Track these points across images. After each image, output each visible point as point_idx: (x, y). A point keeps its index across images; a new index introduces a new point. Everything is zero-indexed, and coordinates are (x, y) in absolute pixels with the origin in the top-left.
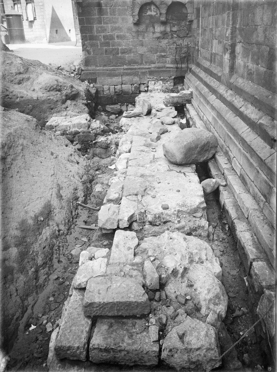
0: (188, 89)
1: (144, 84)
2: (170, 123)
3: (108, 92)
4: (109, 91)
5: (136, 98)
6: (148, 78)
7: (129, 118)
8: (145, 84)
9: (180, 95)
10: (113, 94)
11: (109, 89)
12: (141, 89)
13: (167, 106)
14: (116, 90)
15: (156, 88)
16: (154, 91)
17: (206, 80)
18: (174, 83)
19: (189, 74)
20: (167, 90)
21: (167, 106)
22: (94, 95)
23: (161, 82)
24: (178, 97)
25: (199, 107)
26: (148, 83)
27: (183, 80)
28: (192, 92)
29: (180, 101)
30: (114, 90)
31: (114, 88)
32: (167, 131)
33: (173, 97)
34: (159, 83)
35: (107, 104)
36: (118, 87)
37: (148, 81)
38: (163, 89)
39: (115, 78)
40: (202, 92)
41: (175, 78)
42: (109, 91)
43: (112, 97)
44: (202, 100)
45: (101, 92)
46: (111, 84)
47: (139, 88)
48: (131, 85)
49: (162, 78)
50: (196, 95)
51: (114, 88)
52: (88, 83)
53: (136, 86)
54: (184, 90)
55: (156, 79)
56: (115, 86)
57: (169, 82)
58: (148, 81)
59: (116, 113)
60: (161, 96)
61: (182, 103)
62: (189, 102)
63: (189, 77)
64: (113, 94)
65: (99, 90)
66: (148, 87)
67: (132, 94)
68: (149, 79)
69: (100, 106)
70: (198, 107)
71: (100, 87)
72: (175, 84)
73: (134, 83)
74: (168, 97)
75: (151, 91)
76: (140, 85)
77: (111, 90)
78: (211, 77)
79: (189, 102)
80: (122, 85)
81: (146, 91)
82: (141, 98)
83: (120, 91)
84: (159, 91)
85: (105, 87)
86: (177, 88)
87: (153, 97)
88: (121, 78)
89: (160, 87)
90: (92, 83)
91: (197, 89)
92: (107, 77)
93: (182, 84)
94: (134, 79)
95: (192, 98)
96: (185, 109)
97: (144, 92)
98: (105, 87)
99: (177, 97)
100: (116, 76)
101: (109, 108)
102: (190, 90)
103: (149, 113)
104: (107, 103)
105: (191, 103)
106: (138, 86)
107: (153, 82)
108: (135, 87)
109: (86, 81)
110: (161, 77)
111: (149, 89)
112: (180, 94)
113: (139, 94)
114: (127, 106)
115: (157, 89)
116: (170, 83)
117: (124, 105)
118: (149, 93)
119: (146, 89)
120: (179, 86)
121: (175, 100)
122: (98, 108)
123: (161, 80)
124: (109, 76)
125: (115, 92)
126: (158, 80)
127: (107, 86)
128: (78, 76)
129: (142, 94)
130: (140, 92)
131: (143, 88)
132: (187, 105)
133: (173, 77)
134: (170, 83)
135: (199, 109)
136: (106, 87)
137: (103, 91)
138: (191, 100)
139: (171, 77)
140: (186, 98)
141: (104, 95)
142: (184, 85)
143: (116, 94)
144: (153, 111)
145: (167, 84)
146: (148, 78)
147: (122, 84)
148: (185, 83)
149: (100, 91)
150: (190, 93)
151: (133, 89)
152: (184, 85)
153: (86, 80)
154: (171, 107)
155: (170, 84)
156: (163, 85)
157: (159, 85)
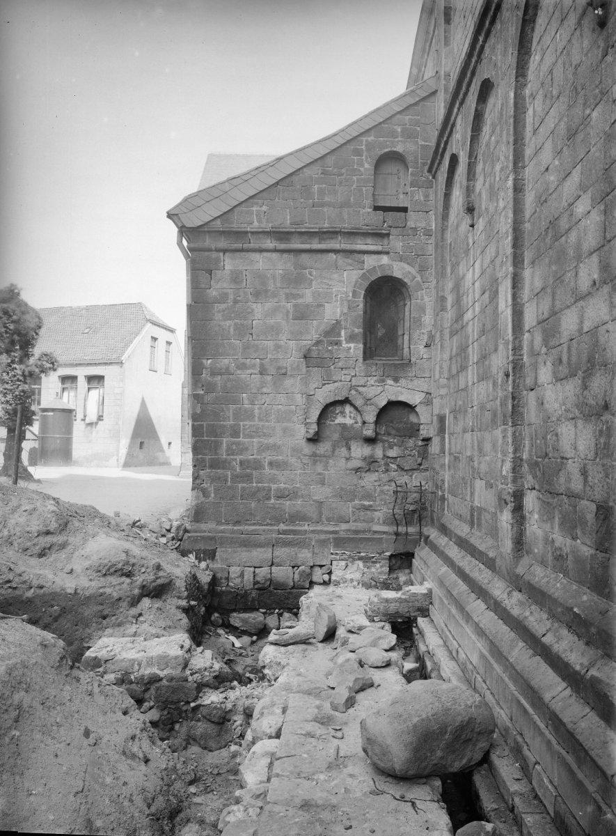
0: (421, 584)
1: (321, 566)
2: (379, 665)
3: (238, 581)
4: (240, 579)
5: (302, 598)
6: (332, 554)
7: (283, 646)
8: (324, 566)
9: (403, 597)
10: (249, 586)
11: (242, 575)
12: (315, 579)
13: (374, 621)
14: (258, 579)
15: (348, 577)
16: (344, 582)
17: (461, 564)
18: (389, 567)
19: (423, 548)
20: (373, 583)
21: (374, 621)
22: (206, 587)
23: (361, 564)
24: (400, 600)
25: (446, 626)
26: (331, 565)
27: (411, 563)
28: (430, 591)
29: (403, 609)
30: (252, 578)
31: (254, 572)
32: (372, 685)
33: (387, 601)
34: (355, 566)
35: (234, 610)
36: (263, 573)
37: (332, 561)
38: (366, 579)
39: (258, 549)
40: (454, 593)
41: (391, 556)
42: (240, 579)
43: (246, 595)
44: (454, 611)
45: (223, 581)
46: (248, 565)
47: (310, 574)
48: (293, 567)
49: (362, 554)
50: (440, 598)
51: (254, 572)
52: (196, 558)
53: (304, 571)
54: (412, 585)
55: (350, 557)
56: (255, 567)
57: (378, 565)
58: (332, 561)
59: (253, 631)
60: (360, 596)
61: (407, 615)
62: (425, 612)
63: (423, 555)
64: (249, 586)
65: (219, 575)
66: (330, 573)
67: (293, 587)
68: (332, 556)
69: (216, 615)
70: (444, 627)
71: (223, 570)
72: (391, 570)
73: (299, 564)
74: (376, 600)
75: (337, 584)
76: (312, 567)
77: (246, 577)
78: (473, 559)
79: (425, 612)
80: (273, 568)
81: (325, 583)
82: (312, 599)
83: (266, 580)
84: (355, 583)
85: (232, 569)
86: (397, 578)
87: (340, 597)
88: (270, 550)
89: (357, 576)
90: (205, 560)
91: (441, 583)
92: (240, 546)
93: (407, 571)
94: (300, 555)
95: (431, 603)
96: (415, 630)
97: (320, 584)
98: (232, 569)
99: (396, 600)
100: (261, 546)
101: (236, 619)
102: (427, 585)
103: (330, 636)
104: (234, 607)
105: (429, 615)
106: (308, 570)
107: (343, 563)
108: (301, 574)
109: (191, 556)
110: (360, 553)
111: (333, 578)
112: (403, 594)
113: (308, 589)
114: (280, 615)
115: (352, 580)
116: (381, 567)
117: (273, 613)
118: (331, 588)
119: (326, 577)
120: (400, 575)
121: (393, 608)
122: (213, 618)
123: (360, 559)
124: (245, 546)
125: (256, 583)
126: (354, 560)
127: (238, 568)
128: (174, 542)
129: (317, 589)
130: (312, 584)
131: (318, 575)
132: (420, 620)
133: (388, 554)
134: (381, 567)
135: (448, 633)
136: (235, 571)
137: (227, 579)
138: (428, 610)
139: (383, 552)
140: (417, 604)
141: (228, 589)
142: (411, 573)
143: (256, 587)
144: (341, 632)
145: (373, 570)
146: (332, 554)
147: (272, 565)
148: (414, 568)
149: (221, 578)
150: (425, 592)
151: (297, 577)
152: (411, 573)
153: (191, 552)
154: (383, 623)
155: (380, 570)
156: (366, 570)
157: (356, 571)
